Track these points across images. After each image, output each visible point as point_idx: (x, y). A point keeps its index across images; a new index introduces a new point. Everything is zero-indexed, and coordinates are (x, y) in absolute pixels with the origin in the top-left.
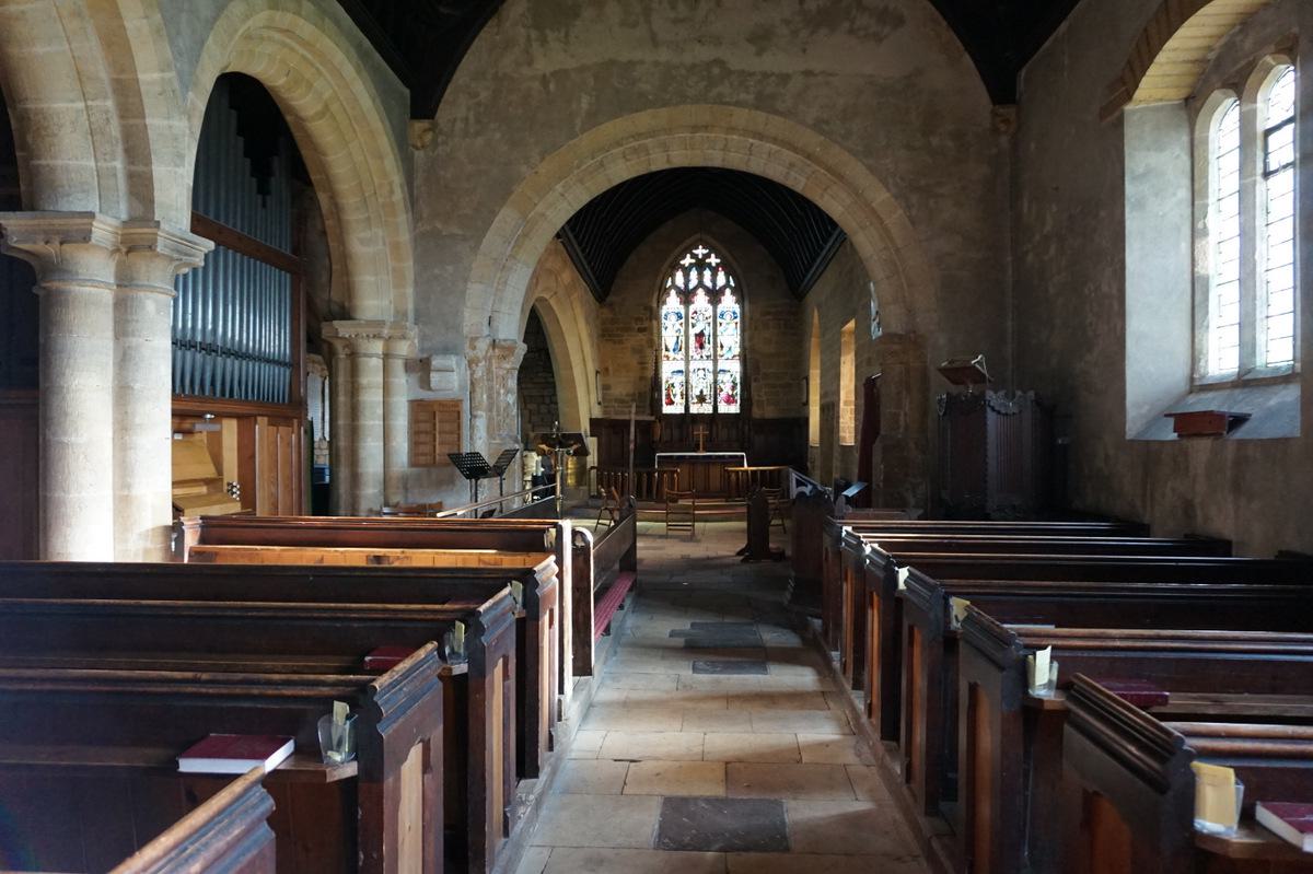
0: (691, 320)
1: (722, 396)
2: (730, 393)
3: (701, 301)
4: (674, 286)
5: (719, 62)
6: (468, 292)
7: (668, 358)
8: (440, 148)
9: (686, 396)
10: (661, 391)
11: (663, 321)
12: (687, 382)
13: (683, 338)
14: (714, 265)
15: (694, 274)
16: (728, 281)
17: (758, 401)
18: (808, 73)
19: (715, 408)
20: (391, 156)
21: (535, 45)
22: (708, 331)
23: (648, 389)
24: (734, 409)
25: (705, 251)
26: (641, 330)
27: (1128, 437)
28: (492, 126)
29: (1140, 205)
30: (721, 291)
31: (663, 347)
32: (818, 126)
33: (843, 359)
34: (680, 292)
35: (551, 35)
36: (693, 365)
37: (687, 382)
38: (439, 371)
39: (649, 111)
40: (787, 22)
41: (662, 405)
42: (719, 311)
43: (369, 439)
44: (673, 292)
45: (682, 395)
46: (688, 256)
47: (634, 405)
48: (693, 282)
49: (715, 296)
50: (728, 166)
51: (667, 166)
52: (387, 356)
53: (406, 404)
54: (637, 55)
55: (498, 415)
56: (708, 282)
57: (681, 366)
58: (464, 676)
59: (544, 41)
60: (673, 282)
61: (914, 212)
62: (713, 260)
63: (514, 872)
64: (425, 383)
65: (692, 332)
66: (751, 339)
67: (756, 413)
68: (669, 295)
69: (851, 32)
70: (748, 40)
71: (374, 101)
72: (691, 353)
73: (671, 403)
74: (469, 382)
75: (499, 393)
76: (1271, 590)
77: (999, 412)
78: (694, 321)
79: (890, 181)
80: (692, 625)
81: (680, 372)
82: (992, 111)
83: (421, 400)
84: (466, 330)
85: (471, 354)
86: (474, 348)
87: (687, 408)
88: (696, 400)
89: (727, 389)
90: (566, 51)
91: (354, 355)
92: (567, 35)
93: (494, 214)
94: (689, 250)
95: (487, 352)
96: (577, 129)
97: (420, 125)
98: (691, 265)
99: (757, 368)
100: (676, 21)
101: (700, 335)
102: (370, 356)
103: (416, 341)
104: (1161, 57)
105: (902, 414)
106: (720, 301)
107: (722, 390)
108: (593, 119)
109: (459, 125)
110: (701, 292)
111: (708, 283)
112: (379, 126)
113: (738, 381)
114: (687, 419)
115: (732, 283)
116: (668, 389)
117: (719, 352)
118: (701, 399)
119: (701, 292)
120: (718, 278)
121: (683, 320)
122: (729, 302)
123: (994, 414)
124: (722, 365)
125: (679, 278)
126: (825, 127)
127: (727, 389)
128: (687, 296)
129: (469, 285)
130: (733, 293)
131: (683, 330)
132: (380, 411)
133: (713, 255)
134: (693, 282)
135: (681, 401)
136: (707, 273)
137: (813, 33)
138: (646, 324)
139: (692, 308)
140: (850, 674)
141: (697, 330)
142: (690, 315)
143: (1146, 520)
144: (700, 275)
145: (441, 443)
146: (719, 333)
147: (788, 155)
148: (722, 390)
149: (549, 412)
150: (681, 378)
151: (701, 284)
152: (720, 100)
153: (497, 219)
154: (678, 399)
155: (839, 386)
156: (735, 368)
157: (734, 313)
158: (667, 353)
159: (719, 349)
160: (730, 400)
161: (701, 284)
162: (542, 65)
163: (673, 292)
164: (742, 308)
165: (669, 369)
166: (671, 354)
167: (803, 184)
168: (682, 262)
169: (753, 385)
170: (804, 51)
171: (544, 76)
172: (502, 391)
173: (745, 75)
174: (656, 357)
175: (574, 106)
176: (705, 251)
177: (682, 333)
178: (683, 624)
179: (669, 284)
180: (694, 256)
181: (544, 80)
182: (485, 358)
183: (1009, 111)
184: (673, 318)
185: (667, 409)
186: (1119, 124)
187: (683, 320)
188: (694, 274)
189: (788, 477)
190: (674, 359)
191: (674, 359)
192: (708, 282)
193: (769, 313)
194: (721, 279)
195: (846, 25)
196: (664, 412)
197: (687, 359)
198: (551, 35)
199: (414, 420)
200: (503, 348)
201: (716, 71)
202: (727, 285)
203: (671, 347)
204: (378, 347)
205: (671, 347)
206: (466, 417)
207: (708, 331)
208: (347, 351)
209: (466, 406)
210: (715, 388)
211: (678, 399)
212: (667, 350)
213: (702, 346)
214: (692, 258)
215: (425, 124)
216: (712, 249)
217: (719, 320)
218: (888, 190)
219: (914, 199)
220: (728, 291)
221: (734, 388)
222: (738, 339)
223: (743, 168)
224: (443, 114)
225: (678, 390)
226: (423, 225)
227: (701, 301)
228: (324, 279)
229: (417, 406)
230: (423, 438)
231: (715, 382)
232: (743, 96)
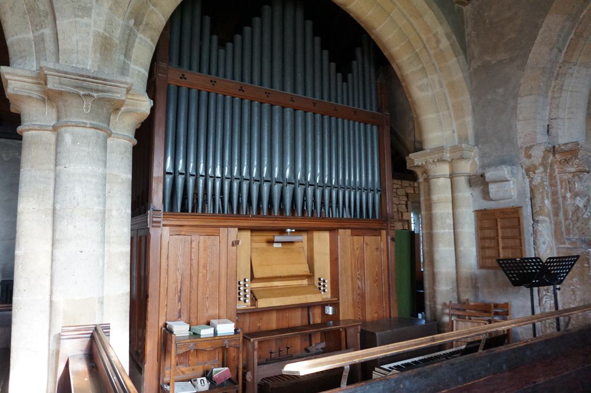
43: (441, 245)
52: (452, 176)
55: (566, 219)
83: (485, 210)
85: (527, 162)
86: (529, 156)
102: (438, 177)
103: (476, 159)
172: (568, 195)
199: (480, 228)
200: (563, 152)
204: (445, 169)
209: (527, 212)
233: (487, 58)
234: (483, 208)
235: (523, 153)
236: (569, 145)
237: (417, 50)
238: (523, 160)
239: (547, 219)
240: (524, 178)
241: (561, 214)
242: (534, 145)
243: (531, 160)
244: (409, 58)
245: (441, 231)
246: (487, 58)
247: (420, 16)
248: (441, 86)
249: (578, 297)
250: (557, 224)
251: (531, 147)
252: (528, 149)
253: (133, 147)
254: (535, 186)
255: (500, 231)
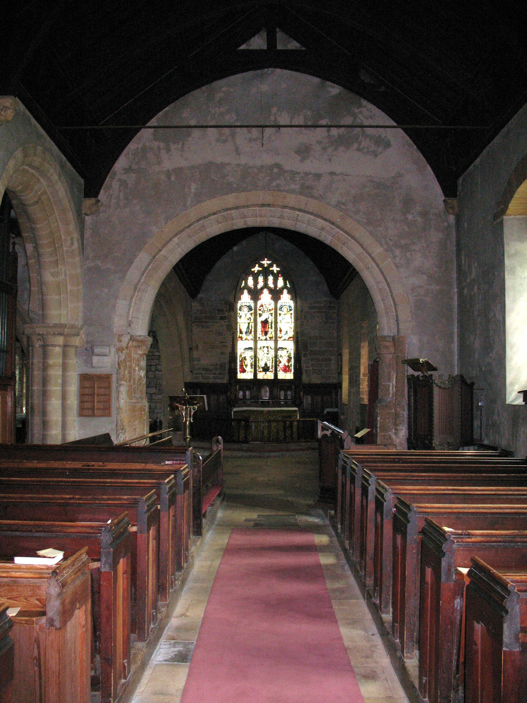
0: (259, 312)
1: (281, 365)
2: (287, 364)
3: (266, 298)
4: (246, 287)
5: (277, 165)
6: (117, 305)
7: (241, 338)
8: (101, 215)
9: (255, 366)
10: (236, 363)
11: (239, 311)
12: (255, 356)
13: (253, 324)
14: (275, 272)
15: (261, 279)
16: (285, 283)
17: (306, 371)
18: (332, 174)
19: (276, 375)
20: (73, 222)
21: (163, 152)
22: (271, 319)
23: (227, 360)
24: (290, 376)
25: (269, 262)
26: (222, 318)
27: (507, 402)
28: (135, 201)
29: (513, 271)
30: (281, 291)
31: (238, 330)
32: (339, 205)
33: (362, 345)
34: (250, 291)
35: (173, 146)
36: (260, 344)
37: (255, 356)
38: (98, 355)
39: (234, 194)
40: (320, 143)
41: (237, 373)
42: (279, 306)
43: (53, 399)
44: (246, 292)
45: (251, 365)
46: (257, 265)
47: (101, 210)
48: (261, 284)
49: (276, 294)
50: (283, 226)
51: (245, 227)
52: (65, 346)
53: (77, 377)
54: (226, 160)
55: (134, 384)
56: (271, 284)
57: (251, 344)
58: (136, 533)
59: (168, 150)
60: (246, 283)
61: (398, 260)
62: (275, 269)
63: (130, 702)
64: (89, 362)
65: (260, 320)
66: (302, 325)
67: (305, 379)
68: (243, 293)
69: (358, 150)
70: (296, 152)
71: (66, 192)
72: (258, 336)
73: (243, 371)
74: (117, 363)
75: (135, 370)
76: (506, 476)
77: (440, 387)
78: (261, 312)
79: (383, 241)
80: (258, 516)
81: (250, 348)
82: (444, 201)
83: (86, 374)
84: (115, 330)
85: (119, 345)
86: (120, 341)
87: (255, 375)
88: (261, 370)
89: (284, 361)
90: (182, 156)
91: (45, 346)
92: (183, 147)
93: (135, 256)
94: (257, 261)
95: (128, 343)
96: (189, 203)
97: (89, 202)
98: (259, 272)
99: (305, 347)
100: (250, 140)
101: (265, 323)
102: (55, 346)
103: (83, 336)
104: (516, 195)
105: (391, 384)
106: (279, 298)
107: (280, 362)
108: (199, 198)
109: (114, 201)
110: (266, 291)
111: (271, 285)
112: (67, 205)
113: (292, 356)
114: (256, 383)
115: (288, 285)
116: (241, 361)
117: (279, 335)
118: (266, 369)
119: (266, 291)
120: (279, 281)
121: (253, 311)
122: (286, 299)
123: (438, 388)
124: (280, 344)
125: (250, 282)
126: (343, 207)
127: (284, 361)
128: (255, 294)
129: (118, 301)
130: (289, 293)
131: (252, 318)
132: (60, 381)
133: (275, 265)
134: (261, 284)
135: (251, 370)
136: (271, 278)
137: (336, 149)
138: (226, 314)
139: (259, 303)
140: (347, 533)
141: (263, 318)
142: (258, 308)
143: (513, 450)
144: (266, 280)
145: (98, 402)
146: (278, 321)
147: (320, 222)
148: (280, 362)
149: (155, 377)
150: (251, 353)
151: (266, 286)
152: (278, 188)
153: (136, 260)
154: (249, 369)
155: (359, 363)
156: (290, 346)
157: (290, 307)
158: (241, 335)
159: (278, 332)
160: (286, 369)
161: (266, 286)
162: (167, 165)
163: (246, 292)
164: (296, 303)
165: (241, 346)
166: (244, 336)
167: (329, 240)
168: (253, 270)
169: (303, 358)
170: (330, 160)
171: (168, 171)
172: (137, 368)
173: (293, 173)
174: (233, 338)
175: (187, 190)
176: (269, 262)
177: (252, 321)
178: (253, 515)
179: (243, 285)
180: (261, 265)
181: (168, 174)
182: (127, 348)
183: (454, 202)
184: (246, 309)
185: (241, 376)
186: (501, 224)
187: (253, 311)
188: (261, 279)
189: (317, 423)
190: (246, 339)
191: (246, 339)
192: (271, 284)
193: (314, 308)
194: (280, 283)
195: (355, 146)
196: (238, 378)
197: (255, 340)
198: (173, 146)
199: (82, 387)
200: (138, 341)
201: (275, 170)
202: (285, 287)
203: (244, 330)
204: (60, 340)
205: (244, 330)
206: (114, 385)
207: (271, 319)
208: (40, 343)
209: (114, 378)
210: (276, 361)
211: (249, 369)
212: (241, 332)
213: (266, 333)
214: (259, 267)
215: (93, 200)
216: (275, 261)
217: (279, 312)
218: (381, 245)
219: (397, 252)
220: (285, 291)
221: (289, 361)
222: (292, 325)
223: (293, 229)
224: (102, 195)
225: (249, 362)
226: (89, 263)
227: (266, 298)
228: (26, 296)
229: (84, 378)
230: (86, 398)
231: (276, 356)
232: (292, 187)
233: (99, 263)
234: (85, 373)
235: (117, 338)
236: (142, 337)
237: (57, 246)
238: (116, 343)
239: (125, 383)
240: (115, 355)
241: (132, 381)
242: (123, 334)
243: (121, 344)
244: (51, 251)
245: (54, 388)
246: (99, 263)
247: (214, 378)
248: (65, 276)
249: (137, 432)
250: (130, 386)
251: (122, 335)
252: (120, 336)
253: (356, 443)
254: (121, 361)
255: (96, 390)
